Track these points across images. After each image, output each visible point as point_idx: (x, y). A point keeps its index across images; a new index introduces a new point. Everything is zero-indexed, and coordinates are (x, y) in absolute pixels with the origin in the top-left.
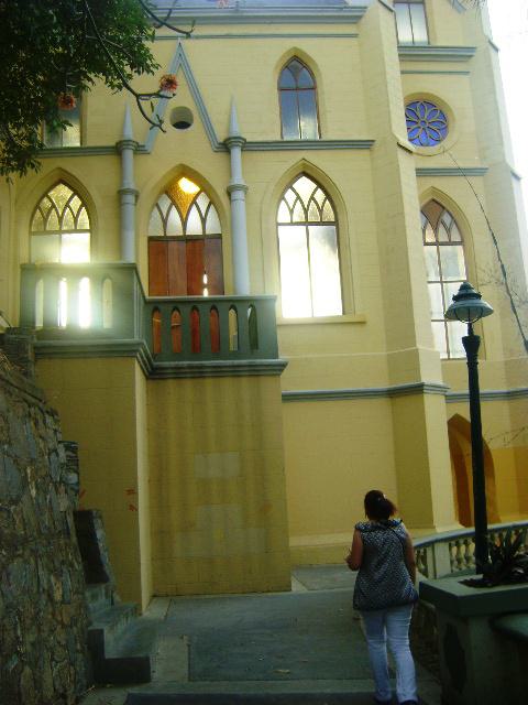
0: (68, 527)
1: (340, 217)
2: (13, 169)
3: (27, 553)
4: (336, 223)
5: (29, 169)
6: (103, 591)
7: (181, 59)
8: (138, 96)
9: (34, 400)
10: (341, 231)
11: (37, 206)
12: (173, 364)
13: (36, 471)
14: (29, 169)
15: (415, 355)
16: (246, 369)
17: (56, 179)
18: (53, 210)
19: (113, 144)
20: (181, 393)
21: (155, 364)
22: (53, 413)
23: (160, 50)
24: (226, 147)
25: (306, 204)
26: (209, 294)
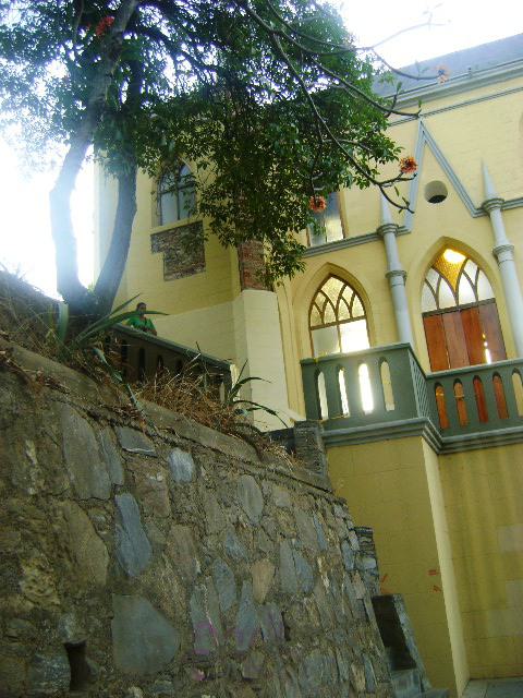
0: (367, 615)
2: (282, 274)
3: (324, 644)
4: (365, 317)
5: (296, 271)
6: (412, 677)
7: (426, 139)
8: (380, 185)
9: (319, 492)
11: (313, 303)
12: (462, 437)
13: (327, 562)
14: (296, 271)
16: (461, 444)
17: (327, 273)
18: (328, 304)
19: (374, 231)
20: (472, 465)
21: (444, 439)
22: (341, 502)
23: (399, 133)
24: (484, 211)
26: (493, 361)
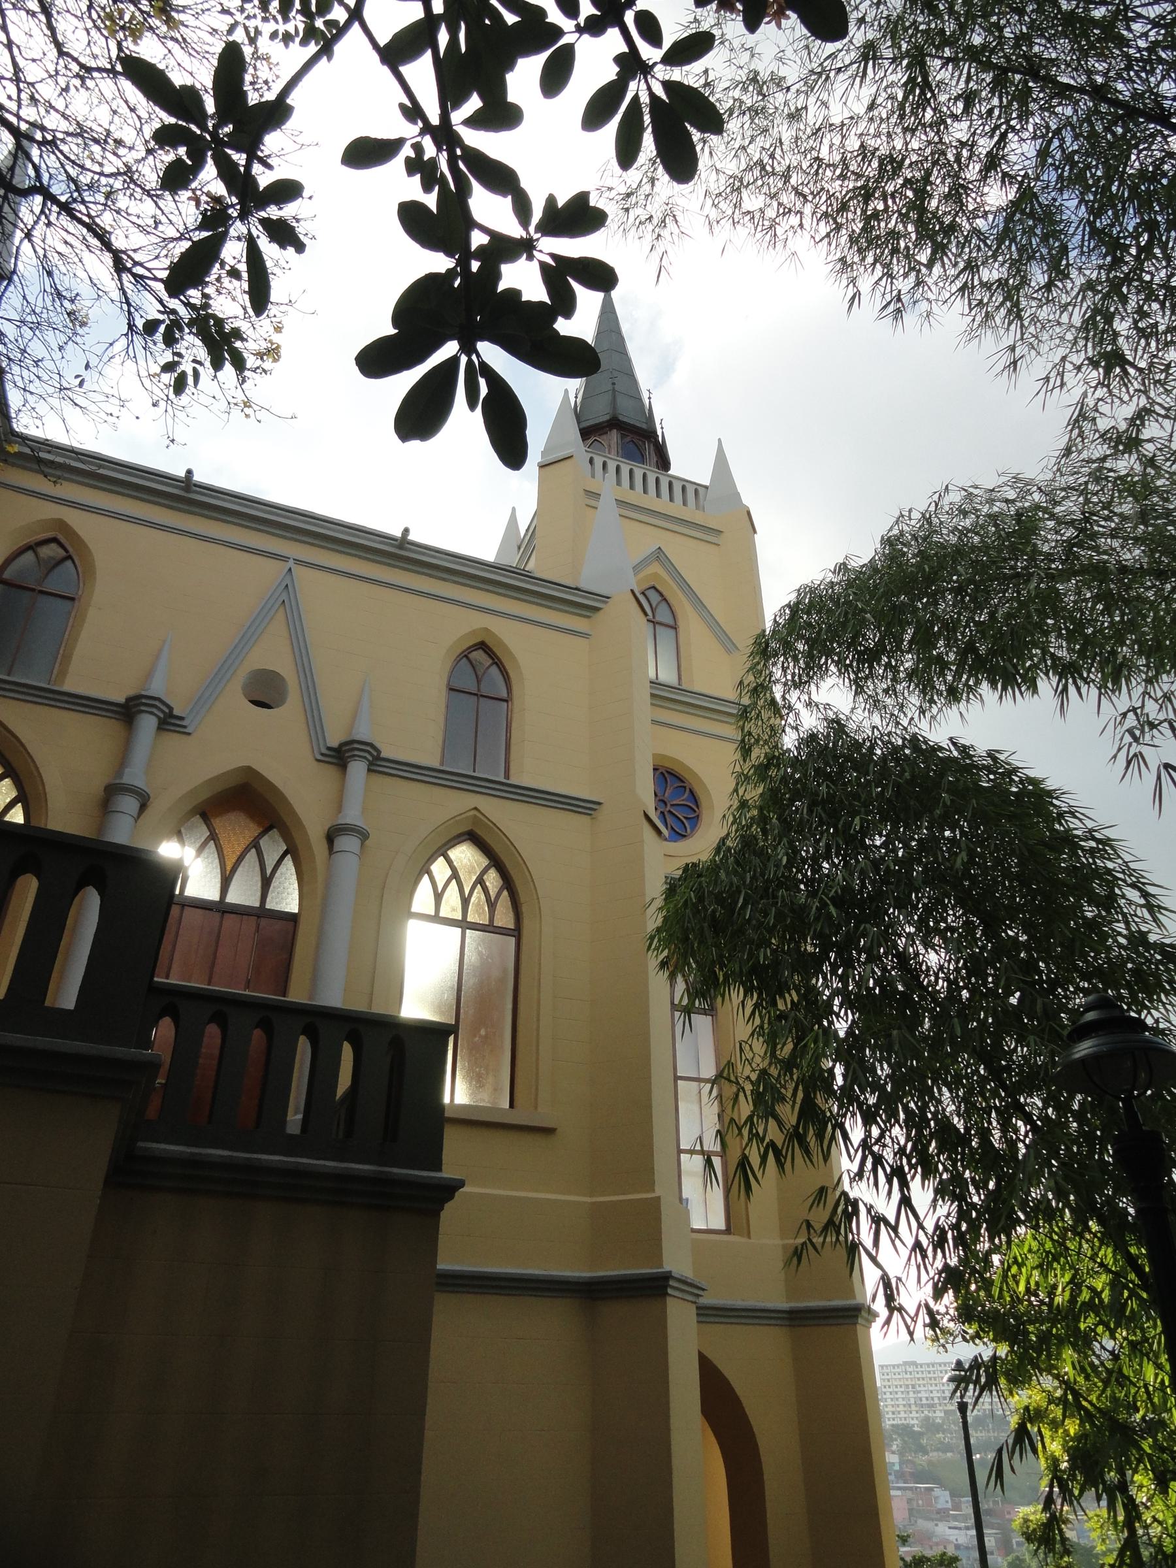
1: (526, 923)
10: (524, 948)
15: (653, 1209)
19: (121, 699)
25: (493, 894)
